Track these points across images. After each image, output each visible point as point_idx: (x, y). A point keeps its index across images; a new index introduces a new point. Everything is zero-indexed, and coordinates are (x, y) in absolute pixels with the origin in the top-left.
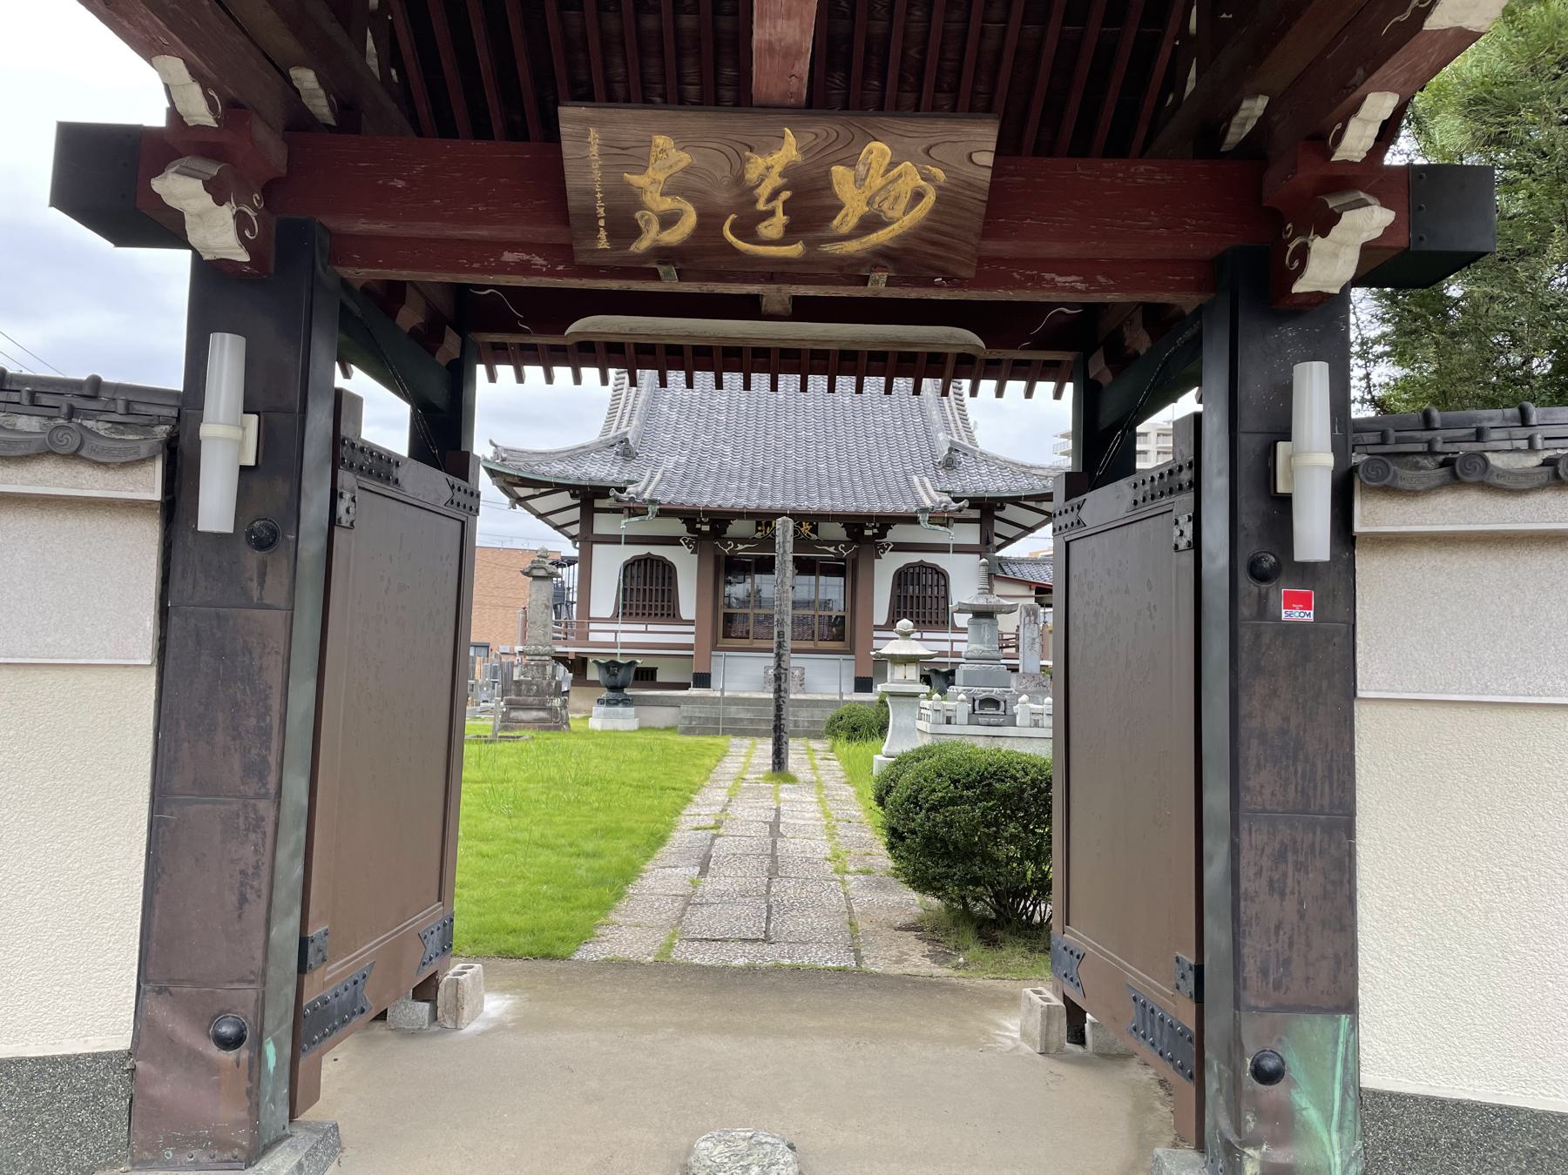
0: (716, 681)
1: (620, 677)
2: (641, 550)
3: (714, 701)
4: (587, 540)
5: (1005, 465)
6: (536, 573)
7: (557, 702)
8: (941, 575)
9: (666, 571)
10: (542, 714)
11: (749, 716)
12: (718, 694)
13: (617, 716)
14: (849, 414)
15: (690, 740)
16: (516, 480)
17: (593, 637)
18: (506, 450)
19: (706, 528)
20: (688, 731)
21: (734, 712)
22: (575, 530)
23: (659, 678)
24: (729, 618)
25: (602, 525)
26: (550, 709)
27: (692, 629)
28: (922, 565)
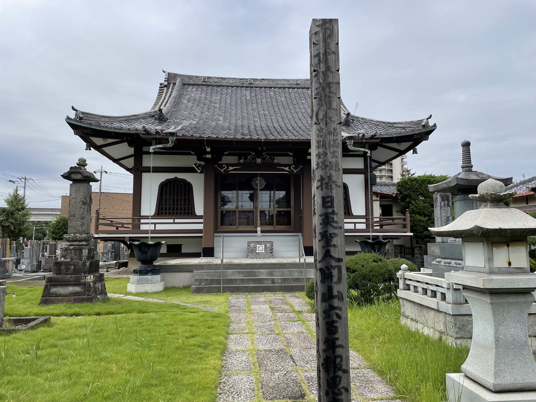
0: (217, 251)
1: (149, 253)
3: (217, 266)
4: (138, 171)
5: (378, 124)
6: (74, 176)
7: (90, 278)
9: (188, 188)
10: (77, 289)
11: (240, 277)
12: (218, 261)
13: (147, 282)
14: (285, 104)
15: (199, 298)
16: (89, 132)
17: (143, 227)
18: (83, 113)
19: (209, 156)
20: (199, 291)
21: (231, 274)
22: (130, 163)
23: (184, 251)
24: (223, 215)
26: (84, 284)
27: (202, 220)
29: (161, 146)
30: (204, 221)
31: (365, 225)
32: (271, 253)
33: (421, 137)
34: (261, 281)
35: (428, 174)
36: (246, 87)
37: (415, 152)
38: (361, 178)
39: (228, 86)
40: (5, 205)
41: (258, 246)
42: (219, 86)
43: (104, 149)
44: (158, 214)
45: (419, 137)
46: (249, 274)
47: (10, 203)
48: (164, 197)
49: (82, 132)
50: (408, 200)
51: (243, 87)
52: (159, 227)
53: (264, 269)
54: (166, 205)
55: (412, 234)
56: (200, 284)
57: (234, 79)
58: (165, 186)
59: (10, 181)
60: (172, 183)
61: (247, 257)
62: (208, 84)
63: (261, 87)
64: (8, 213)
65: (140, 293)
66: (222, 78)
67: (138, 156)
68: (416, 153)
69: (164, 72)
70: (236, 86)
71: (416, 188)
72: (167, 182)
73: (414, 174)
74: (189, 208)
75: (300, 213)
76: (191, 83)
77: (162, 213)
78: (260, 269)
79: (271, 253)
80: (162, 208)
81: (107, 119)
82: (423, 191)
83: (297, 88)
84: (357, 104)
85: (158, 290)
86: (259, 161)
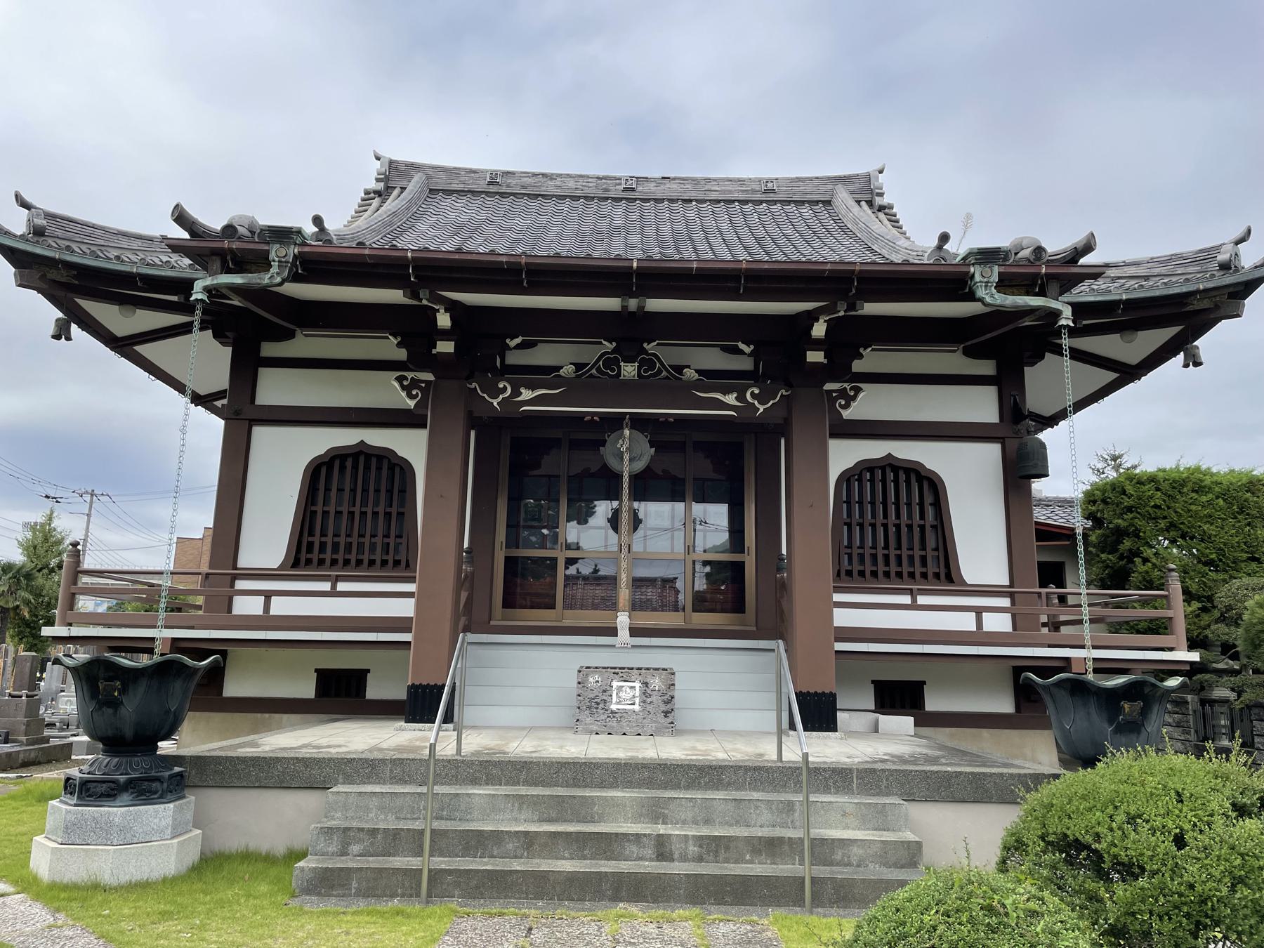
2: (346, 437)
4: (241, 412)
8: (929, 486)
13: (105, 834)
18: (49, 216)
21: (487, 809)
23: (374, 691)
25: (275, 389)
28: (890, 465)
29: (237, 279)
30: (419, 588)
31: (1007, 617)
32: (666, 714)
33: (1217, 307)
34: (607, 845)
35: (1188, 462)
36: (614, 199)
37: (1194, 361)
38: (991, 453)
39: (562, 197)
40: (17, 556)
41: (615, 684)
42: (535, 196)
43: (141, 349)
44: (296, 565)
45: (1205, 304)
46: (562, 809)
47: (31, 549)
48: (319, 508)
49: (43, 278)
50: (1127, 544)
51: (607, 199)
52: (280, 607)
53: (629, 785)
54: (323, 534)
55: (1195, 656)
56: (344, 853)
57: (581, 176)
58: (324, 470)
59: (47, 497)
60: (349, 463)
61: (575, 726)
62: (503, 190)
63: (658, 201)
64: (18, 576)
65: (66, 887)
66: (544, 175)
67: (246, 367)
68: (1197, 364)
69: (378, 158)
70: (586, 198)
71: (1156, 506)
72: (333, 458)
73: (1135, 467)
74: (397, 546)
75: (779, 570)
76: (454, 187)
77: (309, 562)
78: (613, 785)
79: (666, 714)
80: (310, 545)
81: (139, 243)
82: (1180, 515)
83: (767, 202)
84: (969, 216)
85: (156, 875)
86: (629, 370)
